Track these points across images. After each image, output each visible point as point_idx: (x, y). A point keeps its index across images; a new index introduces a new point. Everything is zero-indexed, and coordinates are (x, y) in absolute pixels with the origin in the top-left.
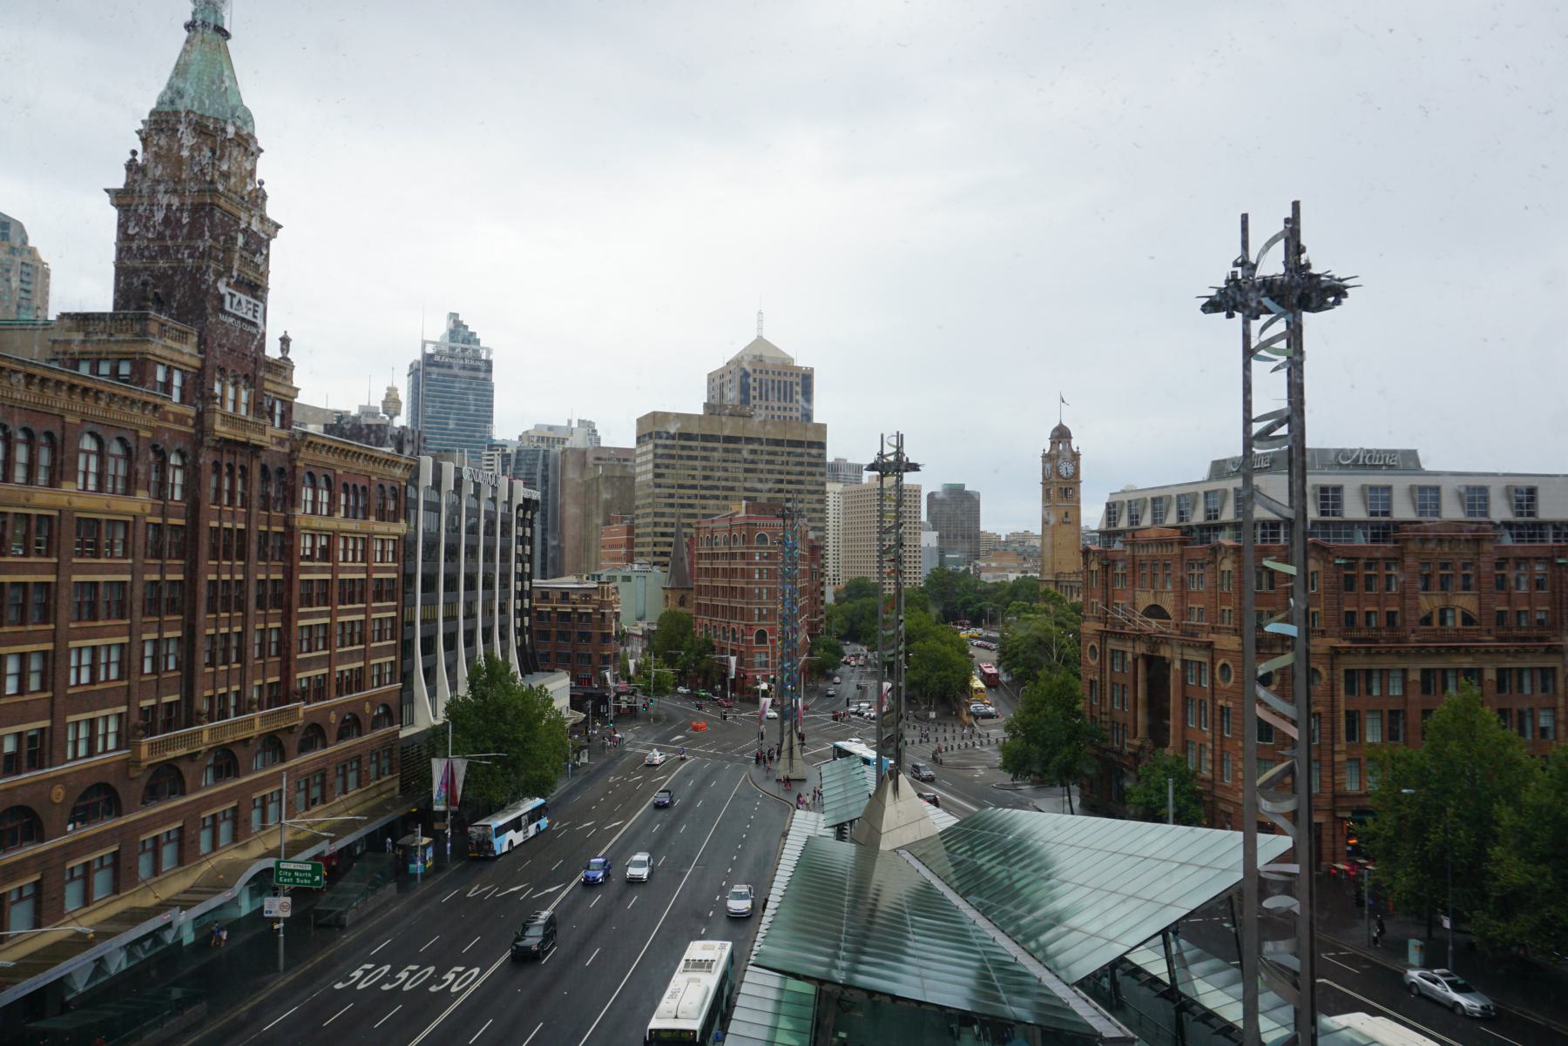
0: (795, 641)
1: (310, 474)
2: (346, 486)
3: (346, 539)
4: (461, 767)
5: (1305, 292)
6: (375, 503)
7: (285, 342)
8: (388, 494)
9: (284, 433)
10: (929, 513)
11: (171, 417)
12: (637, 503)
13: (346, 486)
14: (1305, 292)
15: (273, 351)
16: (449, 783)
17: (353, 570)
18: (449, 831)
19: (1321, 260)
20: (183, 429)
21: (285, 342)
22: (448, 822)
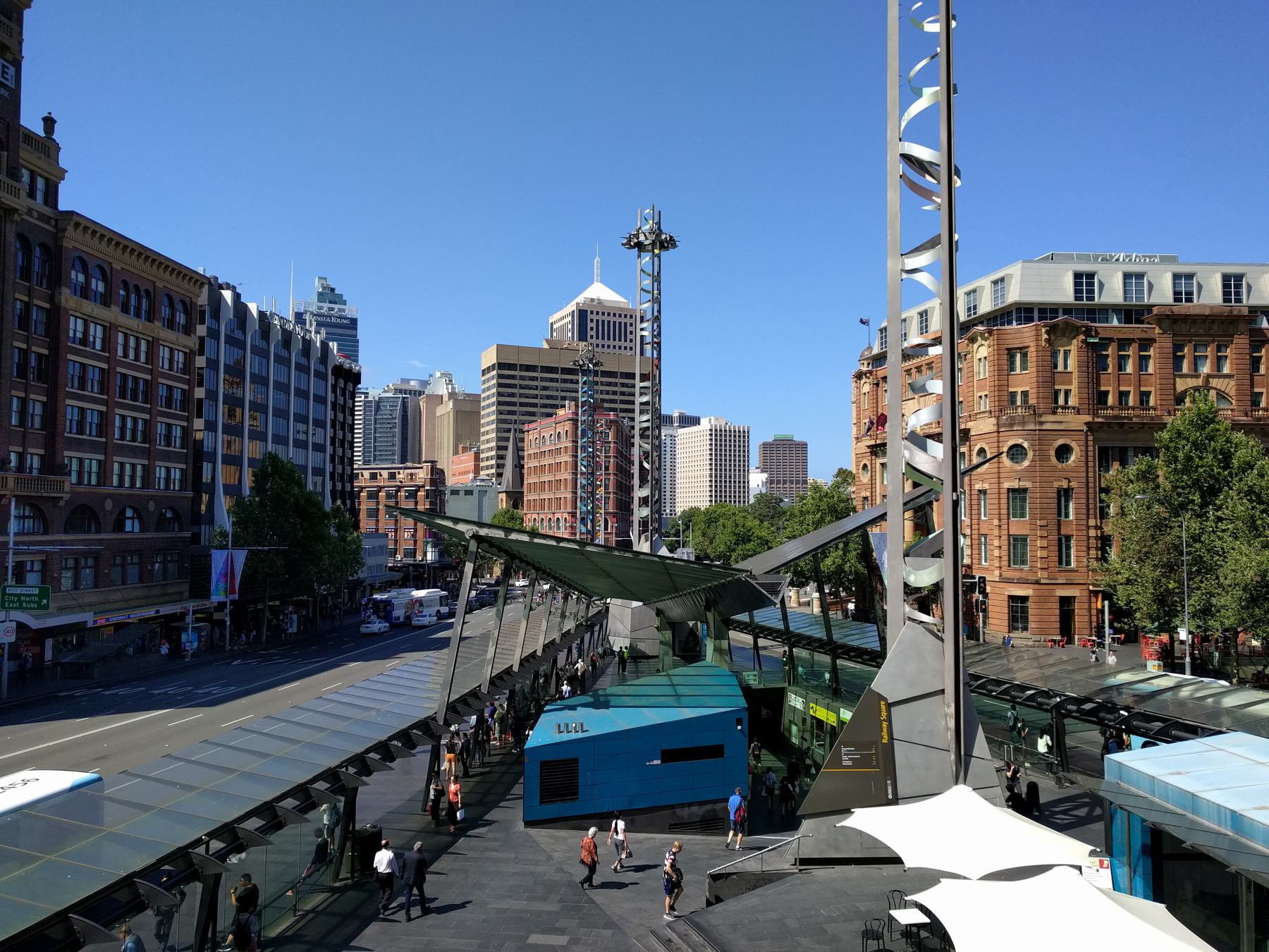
0: (224, 535)
1: (169, 296)
2: (125, 282)
3: (126, 335)
4: (240, 557)
5: (664, 243)
6: (165, 311)
7: (49, 122)
8: (143, 293)
9: (47, 211)
10: (517, 541)
11: (35, 214)
12: (482, 430)
13: (125, 282)
14: (664, 243)
15: (31, 120)
16: (229, 574)
17: (138, 369)
18: (228, 619)
19: (668, 230)
20: (49, 228)
21: (49, 122)
22: (227, 611)
